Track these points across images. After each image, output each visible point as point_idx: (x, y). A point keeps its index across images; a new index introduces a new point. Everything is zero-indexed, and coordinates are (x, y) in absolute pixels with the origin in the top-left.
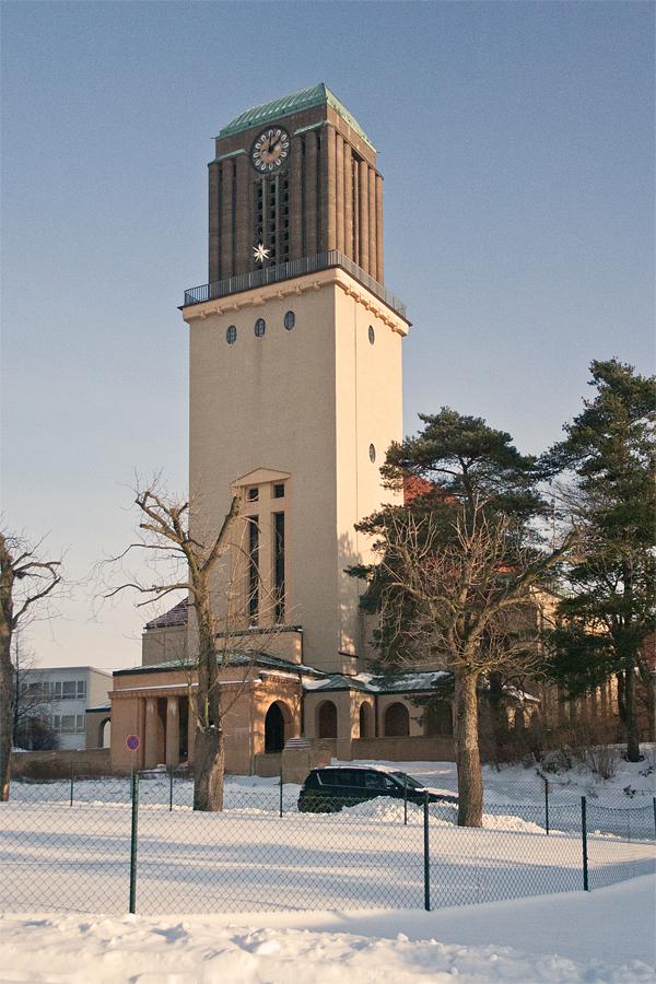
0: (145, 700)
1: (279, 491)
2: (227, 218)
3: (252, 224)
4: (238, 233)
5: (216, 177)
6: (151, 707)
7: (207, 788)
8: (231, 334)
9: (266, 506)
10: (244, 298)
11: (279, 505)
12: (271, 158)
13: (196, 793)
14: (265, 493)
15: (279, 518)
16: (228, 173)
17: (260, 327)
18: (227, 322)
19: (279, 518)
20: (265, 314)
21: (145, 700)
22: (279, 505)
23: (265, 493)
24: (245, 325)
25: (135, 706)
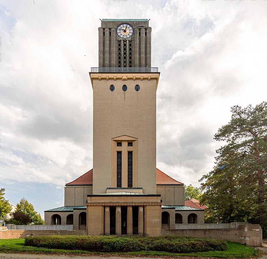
0: (105, 207)
1: (130, 144)
2: (107, 49)
3: (133, 47)
4: (112, 55)
5: (102, 35)
6: (108, 210)
7: (244, 144)
8: (112, 88)
9: (125, 149)
10: (119, 76)
11: (130, 149)
12: (125, 34)
13: (73, 226)
14: (124, 144)
15: (130, 153)
16: (107, 33)
17: (125, 88)
18: (111, 83)
19: (130, 153)
20: (115, 83)
21: (105, 207)
22: (130, 149)
23: (124, 144)
24: (118, 85)
25: (101, 209)
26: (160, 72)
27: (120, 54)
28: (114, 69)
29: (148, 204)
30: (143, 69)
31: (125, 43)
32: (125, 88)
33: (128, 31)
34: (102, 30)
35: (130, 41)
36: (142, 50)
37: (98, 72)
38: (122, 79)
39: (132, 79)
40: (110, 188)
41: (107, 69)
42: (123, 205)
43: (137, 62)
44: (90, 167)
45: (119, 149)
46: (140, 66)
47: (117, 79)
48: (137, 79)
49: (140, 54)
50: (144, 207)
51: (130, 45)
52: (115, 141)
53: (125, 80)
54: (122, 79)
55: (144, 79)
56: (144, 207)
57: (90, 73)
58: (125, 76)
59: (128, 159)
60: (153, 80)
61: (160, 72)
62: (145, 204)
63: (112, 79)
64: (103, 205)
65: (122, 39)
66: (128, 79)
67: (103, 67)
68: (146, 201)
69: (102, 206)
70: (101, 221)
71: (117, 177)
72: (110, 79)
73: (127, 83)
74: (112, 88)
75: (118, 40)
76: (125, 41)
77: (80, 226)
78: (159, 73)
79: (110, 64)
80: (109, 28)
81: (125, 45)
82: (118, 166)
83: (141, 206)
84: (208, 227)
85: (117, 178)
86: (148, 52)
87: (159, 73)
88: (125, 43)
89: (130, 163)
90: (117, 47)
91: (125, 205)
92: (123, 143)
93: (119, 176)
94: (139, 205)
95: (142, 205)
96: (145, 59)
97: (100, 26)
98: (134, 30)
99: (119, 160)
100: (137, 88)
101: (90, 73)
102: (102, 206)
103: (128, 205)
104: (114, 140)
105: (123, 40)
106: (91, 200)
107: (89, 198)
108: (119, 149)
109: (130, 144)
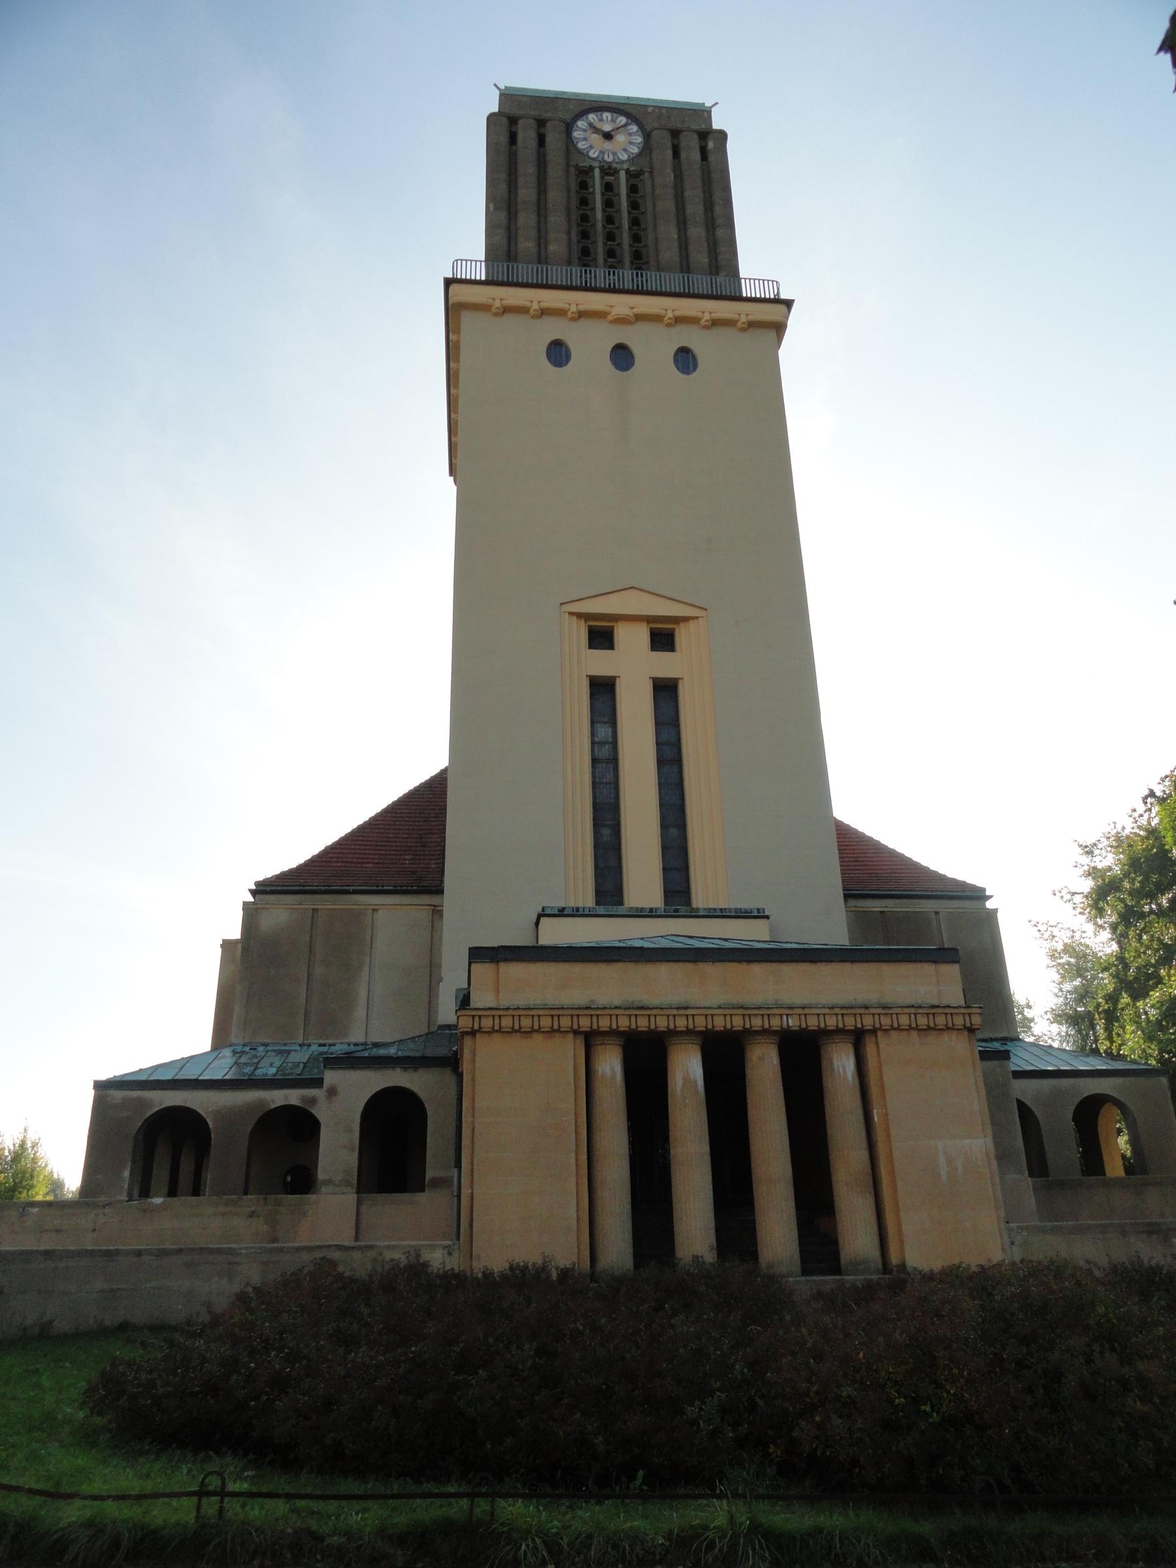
0: (590, 1040)
1: (663, 640)
6: (610, 1064)
11: (665, 665)
12: (608, 145)
18: (552, 329)
22: (665, 665)
25: (569, 1051)
26: (792, 301)
27: (584, 218)
28: (557, 273)
29: (886, 1021)
30: (701, 282)
31: (610, 178)
32: (622, 356)
33: (620, 138)
34: (505, 121)
35: (631, 175)
36: (689, 210)
37: (483, 278)
38: (610, 318)
39: (656, 318)
40: (561, 913)
41: (524, 271)
42: (719, 1024)
43: (669, 253)
44: (447, 765)
45: (601, 663)
46: (686, 267)
47: (582, 315)
48: (679, 320)
49: (682, 223)
50: (858, 1038)
51: (633, 189)
52: (579, 616)
53: (621, 321)
54: (610, 318)
55: (715, 323)
56: (858, 1038)
57: (448, 282)
58: (622, 304)
59: (658, 724)
60: (759, 332)
61: (792, 301)
62: (868, 1022)
63: (559, 313)
64: (585, 1023)
65: (596, 164)
66: (640, 318)
67: (509, 261)
68: (873, 998)
69: (576, 1033)
70: (573, 1161)
71: (595, 833)
72: (544, 312)
73: (633, 337)
74: (558, 353)
75: (577, 167)
76: (608, 170)
77: (364, 1209)
78: (789, 304)
79: (543, 253)
80: (536, 120)
81: (608, 187)
82: (600, 766)
83: (840, 1032)
84: (396, 1487)
85: (596, 846)
86: (719, 221)
87: (789, 304)
88: (610, 178)
89: (605, 751)
90: (573, 194)
91: (738, 1023)
92: (622, 633)
93: (606, 832)
94: (831, 1022)
95: (850, 1023)
96: (709, 245)
97: (496, 109)
98: (647, 136)
99: (604, 732)
100: (685, 359)
101: (448, 282)
102: (576, 1033)
103: (757, 1023)
104: (570, 613)
105: (601, 168)
106: (497, 991)
107: (482, 970)
108: (601, 663)
109: (663, 640)
